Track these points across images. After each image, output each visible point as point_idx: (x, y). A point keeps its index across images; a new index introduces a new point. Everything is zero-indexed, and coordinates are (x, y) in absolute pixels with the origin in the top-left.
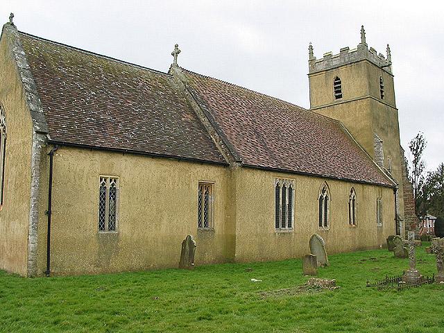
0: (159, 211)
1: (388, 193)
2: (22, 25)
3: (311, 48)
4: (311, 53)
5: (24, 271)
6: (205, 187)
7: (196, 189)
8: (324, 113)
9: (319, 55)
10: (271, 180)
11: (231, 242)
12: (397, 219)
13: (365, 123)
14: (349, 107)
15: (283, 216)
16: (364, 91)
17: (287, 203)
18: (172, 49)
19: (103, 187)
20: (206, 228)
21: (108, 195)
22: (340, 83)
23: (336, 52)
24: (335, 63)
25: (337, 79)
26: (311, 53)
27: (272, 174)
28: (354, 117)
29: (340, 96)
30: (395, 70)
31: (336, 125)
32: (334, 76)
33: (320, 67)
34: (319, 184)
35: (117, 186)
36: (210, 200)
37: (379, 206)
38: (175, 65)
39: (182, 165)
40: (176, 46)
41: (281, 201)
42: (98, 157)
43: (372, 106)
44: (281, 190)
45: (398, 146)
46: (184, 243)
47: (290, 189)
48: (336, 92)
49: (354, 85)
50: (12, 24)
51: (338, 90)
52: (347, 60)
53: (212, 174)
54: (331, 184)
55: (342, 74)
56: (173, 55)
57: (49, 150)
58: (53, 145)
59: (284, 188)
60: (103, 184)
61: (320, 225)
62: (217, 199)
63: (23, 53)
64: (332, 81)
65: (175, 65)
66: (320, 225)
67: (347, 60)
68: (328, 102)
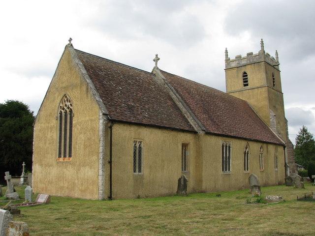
0: (163, 161)
1: (280, 149)
2: (76, 46)
3: (227, 52)
4: (227, 55)
5: (96, 197)
6: (185, 146)
7: (180, 147)
8: (236, 95)
9: (232, 57)
10: (220, 141)
11: (199, 181)
12: (286, 166)
13: (266, 103)
14: (253, 92)
15: (226, 164)
16: (264, 82)
17: (228, 156)
18: (154, 57)
19: (135, 147)
20: (140, 173)
21: (138, 154)
22: (247, 76)
23: (244, 55)
24: (244, 62)
25: (245, 73)
26: (227, 55)
27: (220, 138)
28: (257, 99)
29: (247, 85)
30: (281, 68)
31: (245, 103)
32: (243, 71)
33: (233, 65)
34: (244, 143)
35: (142, 146)
36: (187, 154)
37: (276, 158)
38: (156, 68)
39: (174, 133)
40: (157, 55)
41: (225, 154)
42: (133, 129)
43: (269, 92)
44: (225, 148)
45: (284, 118)
46: (180, 180)
47: (229, 147)
48: (244, 82)
49: (257, 78)
50: (72, 45)
51: (246, 83)
52: (251, 61)
53: (187, 138)
54: (251, 143)
55: (248, 70)
56: (154, 60)
57: (109, 125)
58: (111, 121)
59: (226, 146)
60: (135, 144)
61: (245, 170)
62: (191, 153)
63: (81, 63)
64: (241, 75)
65: (156, 68)
66: (245, 170)
67: (251, 61)
68: (239, 89)
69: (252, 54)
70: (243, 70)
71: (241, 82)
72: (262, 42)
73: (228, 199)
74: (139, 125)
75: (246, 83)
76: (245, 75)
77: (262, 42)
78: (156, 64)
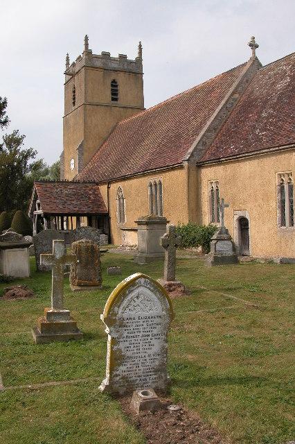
4: (87, 45)
18: (250, 40)
25: (114, 81)
26: (87, 45)
48: (112, 94)
51: (115, 94)
64: (109, 83)
69: (125, 57)
70: (113, 76)
71: (109, 93)
72: (140, 46)
73: (166, 263)
74: (188, 186)
75: (115, 94)
76: (114, 84)
77: (140, 46)
78: (254, 53)
